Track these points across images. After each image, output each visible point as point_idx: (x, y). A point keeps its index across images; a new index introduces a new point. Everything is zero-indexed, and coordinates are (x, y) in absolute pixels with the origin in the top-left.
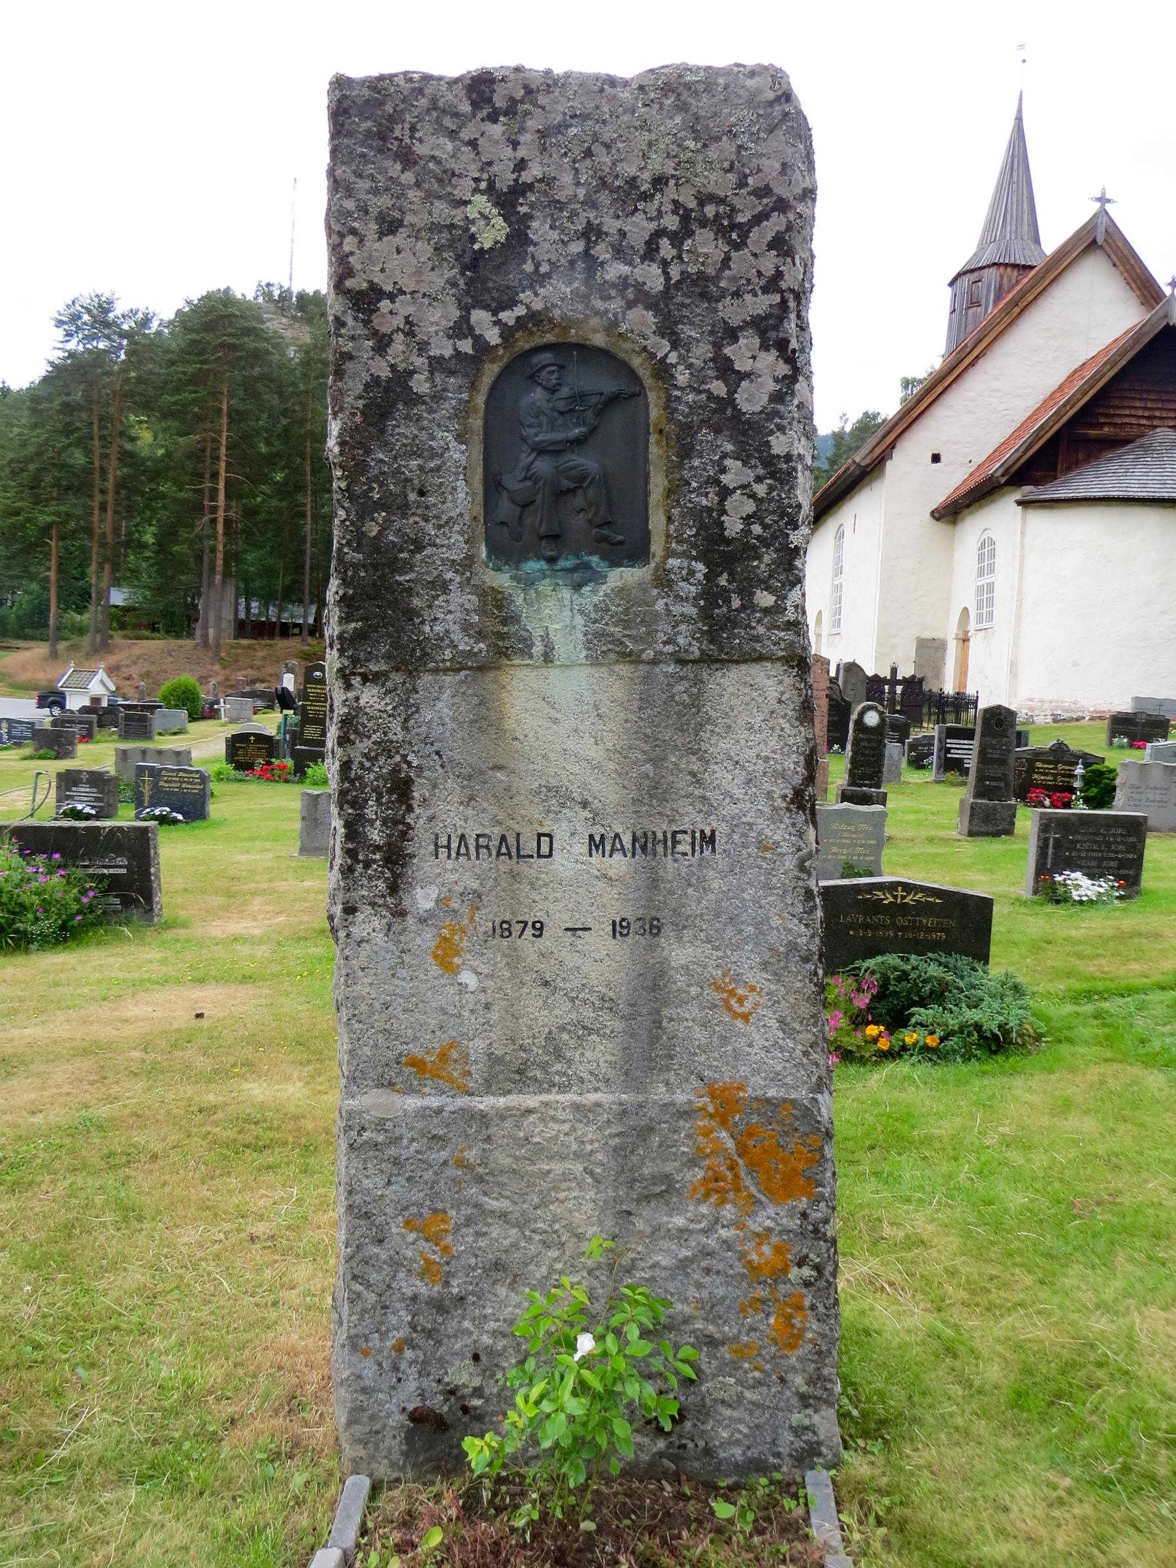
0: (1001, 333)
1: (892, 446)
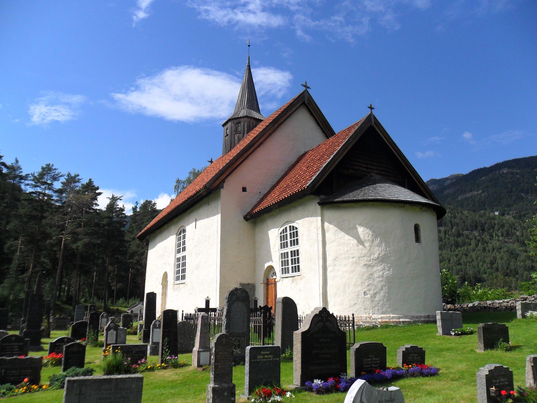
0: (270, 135)
1: (223, 181)
